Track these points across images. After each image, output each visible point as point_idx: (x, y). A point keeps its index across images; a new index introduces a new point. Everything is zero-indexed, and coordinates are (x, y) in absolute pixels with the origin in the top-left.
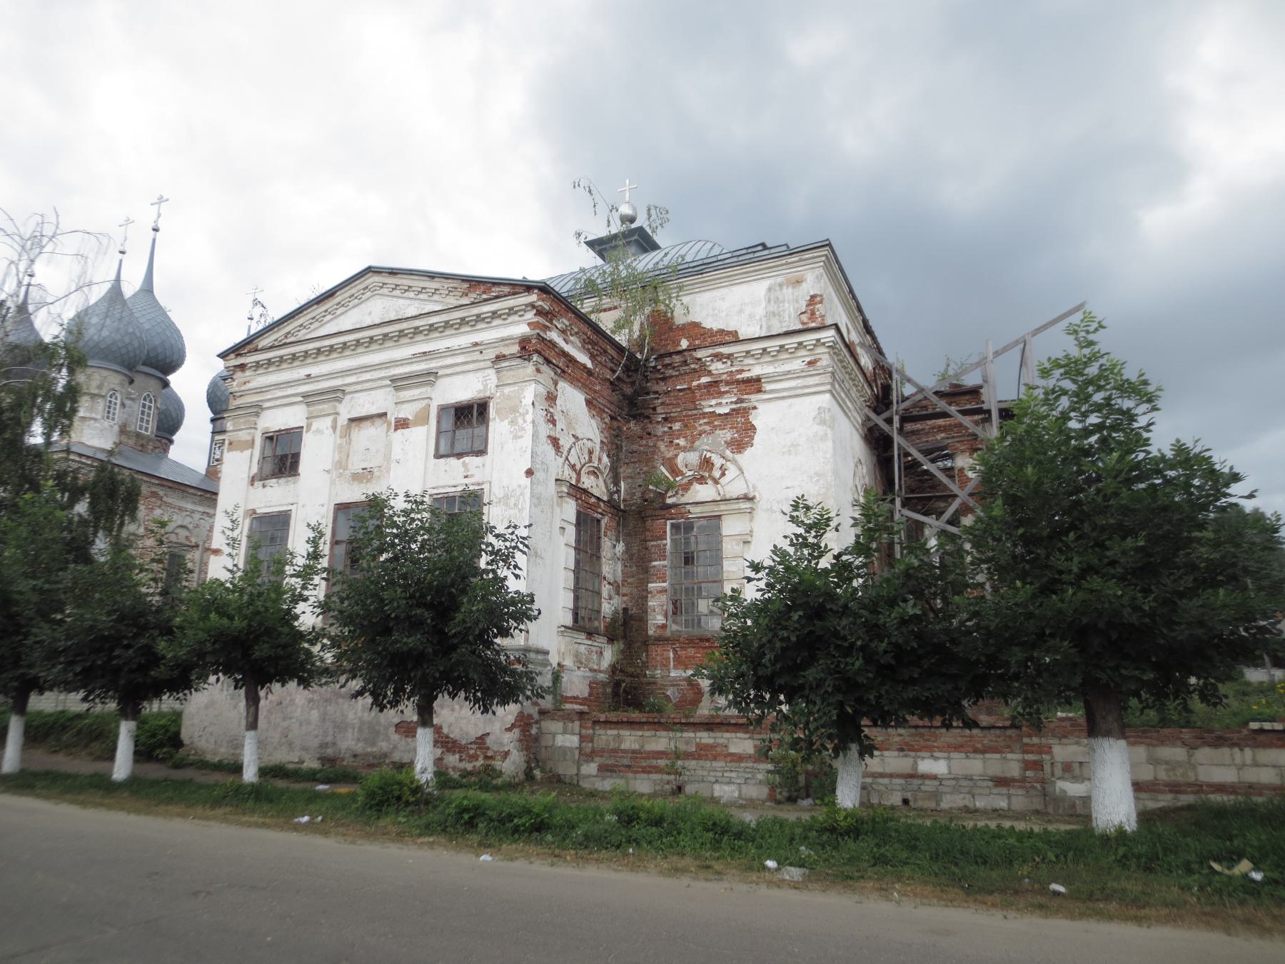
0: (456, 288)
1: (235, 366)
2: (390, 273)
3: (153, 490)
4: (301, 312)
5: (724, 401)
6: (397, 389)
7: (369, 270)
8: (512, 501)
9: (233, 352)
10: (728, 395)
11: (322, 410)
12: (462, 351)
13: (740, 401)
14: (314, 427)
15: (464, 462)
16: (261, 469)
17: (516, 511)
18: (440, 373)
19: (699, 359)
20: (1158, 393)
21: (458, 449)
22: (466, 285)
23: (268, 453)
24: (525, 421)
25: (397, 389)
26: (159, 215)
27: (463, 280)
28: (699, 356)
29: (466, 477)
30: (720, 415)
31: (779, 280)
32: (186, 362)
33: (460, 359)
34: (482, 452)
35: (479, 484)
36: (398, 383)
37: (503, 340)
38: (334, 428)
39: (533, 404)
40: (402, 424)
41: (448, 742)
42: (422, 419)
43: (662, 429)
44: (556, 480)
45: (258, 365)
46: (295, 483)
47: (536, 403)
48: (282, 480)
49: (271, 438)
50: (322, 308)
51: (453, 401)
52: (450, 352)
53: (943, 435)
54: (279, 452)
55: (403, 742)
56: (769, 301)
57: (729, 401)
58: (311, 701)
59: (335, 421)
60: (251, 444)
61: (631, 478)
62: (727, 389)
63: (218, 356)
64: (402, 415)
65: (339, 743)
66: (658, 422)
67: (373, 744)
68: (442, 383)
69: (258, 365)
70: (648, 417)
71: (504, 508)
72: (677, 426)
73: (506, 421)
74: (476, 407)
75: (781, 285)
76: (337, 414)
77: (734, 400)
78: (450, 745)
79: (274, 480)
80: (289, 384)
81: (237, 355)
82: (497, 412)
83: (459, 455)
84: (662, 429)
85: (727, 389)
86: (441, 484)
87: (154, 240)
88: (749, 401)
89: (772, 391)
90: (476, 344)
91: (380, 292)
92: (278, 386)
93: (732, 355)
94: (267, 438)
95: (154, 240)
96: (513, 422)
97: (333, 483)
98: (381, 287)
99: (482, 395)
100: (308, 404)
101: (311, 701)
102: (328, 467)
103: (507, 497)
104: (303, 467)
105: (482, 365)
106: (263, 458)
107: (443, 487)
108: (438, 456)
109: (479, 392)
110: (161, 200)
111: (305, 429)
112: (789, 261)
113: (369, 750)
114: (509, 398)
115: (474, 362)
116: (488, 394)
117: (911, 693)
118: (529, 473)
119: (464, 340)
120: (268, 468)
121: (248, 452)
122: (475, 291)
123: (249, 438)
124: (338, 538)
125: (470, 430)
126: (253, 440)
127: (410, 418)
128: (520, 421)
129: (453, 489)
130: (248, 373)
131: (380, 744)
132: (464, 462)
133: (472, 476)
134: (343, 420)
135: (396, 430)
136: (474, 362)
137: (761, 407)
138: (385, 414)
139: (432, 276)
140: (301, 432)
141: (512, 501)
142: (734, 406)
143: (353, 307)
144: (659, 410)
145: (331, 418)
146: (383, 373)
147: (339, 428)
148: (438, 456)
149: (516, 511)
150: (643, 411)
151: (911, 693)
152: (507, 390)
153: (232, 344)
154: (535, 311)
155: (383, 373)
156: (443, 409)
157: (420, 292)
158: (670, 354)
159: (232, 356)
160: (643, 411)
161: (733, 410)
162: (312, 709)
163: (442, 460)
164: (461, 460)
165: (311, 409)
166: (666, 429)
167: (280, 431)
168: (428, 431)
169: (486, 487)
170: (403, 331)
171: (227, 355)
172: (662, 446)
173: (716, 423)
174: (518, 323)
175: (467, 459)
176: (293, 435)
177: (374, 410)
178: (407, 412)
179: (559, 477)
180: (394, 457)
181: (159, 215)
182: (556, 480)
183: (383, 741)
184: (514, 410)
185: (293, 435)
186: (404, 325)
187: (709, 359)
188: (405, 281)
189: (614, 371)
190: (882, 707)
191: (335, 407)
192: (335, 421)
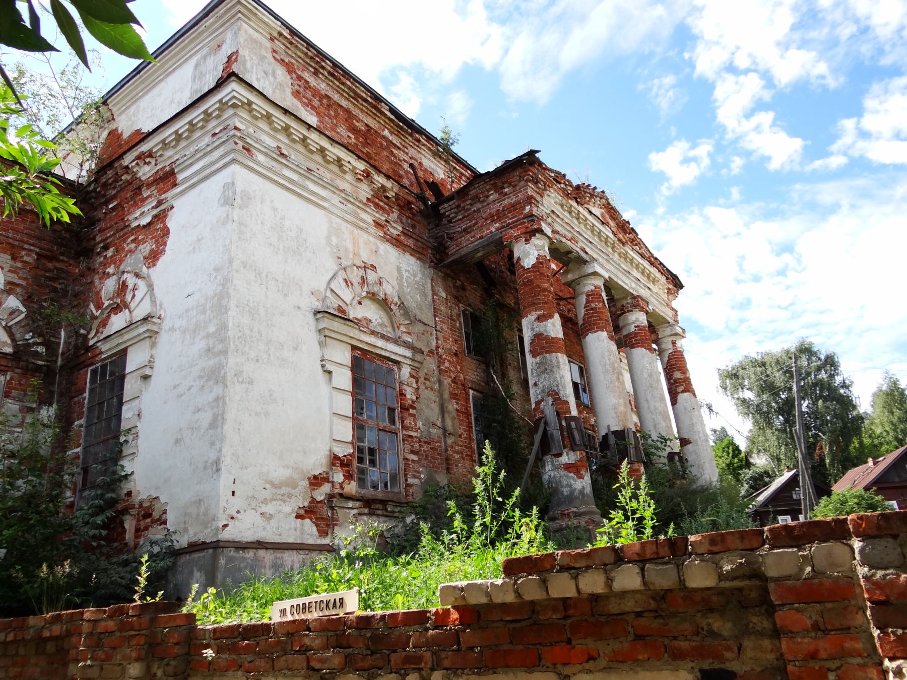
5: (146, 209)
7: (676, 311)
10: (150, 200)
13: (160, 203)
19: (127, 167)
20: (458, 137)
30: (144, 227)
31: (205, 51)
53: (497, 225)
56: (195, 78)
57: (150, 207)
60: (367, 607)
62: (149, 193)
75: (205, 57)
77: (154, 204)
85: (149, 193)
88: (167, 200)
89: (186, 180)
93: (150, 151)
112: (207, 24)
117: (516, 388)
137: (176, 203)
142: (155, 212)
151: (516, 388)
161: (155, 217)
173: (140, 238)
187: (134, 164)
190: (837, 402)
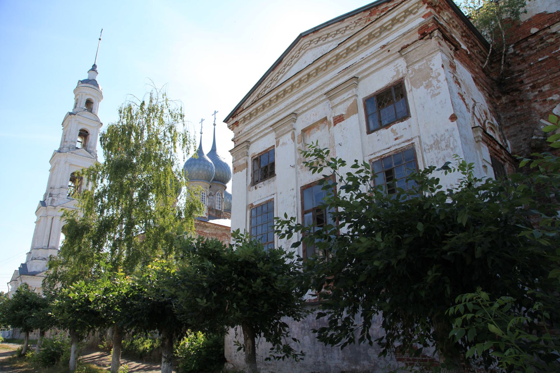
0: (360, 19)
1: (233, 124)
2: (314, 32)
3: (224, 232)
4: (264, 79)
6: (330, 99)
7: (302, 36)
8: (443, 144)
9: (231, 117)
11: (285, 130)
12: (374, 55)
14: (281, 143)
15: (392, 130)
16: (253, 179)
17: (449, 150)
18: (360, 77)
21: (385, 122)
22: (368, 13)
23: (256, 168)
24: (439, 81)
25: (330, 99)
26: (215, 119)
27: (365, 11)
28: (554, 31)
29: (396, 139)
32: (227, 163)
33: (375, 61)
34: (406, 115)
35: (409, 140)
36: (330, 95)
37: (404, 34)
38: (293, 138)
39: (443, 66)
40: (339, 119)
41: (426, 361)
42: (353, 110)
43: (533, 94)
44: (472, 128)
45: (245, 119)
46: (274, 181)
47: (445, 66)
48: (266, 182)
49: (256, 159)
50: (277, 70)
51: (374, 91)
52: (365, 60)
54: (262, 166)
55: (382, 361)
58: (303, 329)
59: (293, 134)
61: (515, 135)
63: (224, 121)
64: (338, 114)
65: (328, 362)
66: (528, 91)
67: (357, 362)
68: (361, 85)
69: (245, 119)
70: (517, 90)
71: (436, 151)
72: (546, 88)
73: (422, 87)
74: (393, 88)
76: (294, 129)
78: (428, 363)
79: (262, 183)
80: (262, 123)
81: (233, 118)
82: (413, 84)
83: (387, 126)
84: (533, 94)
86: (379, 149)
87: (214, 129)
90: (384, 46)
91: (310, 47)
92: (257, 126)
94: (254, 159)
95: (214, 129)
96: (427, 87)
97: (297, 173)
98: (310, 44)
99: (396, 79)
100: (274, 130)
101: (303, 329)
102: (293, 163)
103: (437, 143)
104: (278, 169)
105: (391, 58)
106: (254, 172)
107: (379, 152)
108: (369, 132)
109: (393, 78)
110: (215, 112)
111: (275, 146)
113: (354, 368)
114: (420, 70)
115: (384, 59)
116: (401, 76)
118: (453, 118)
119: (375, 47)
120: (258, 176)
121: (245, 171)
122: (375, 14)
123: (244, 162)
124: (306, 209)
125: (391, 107)
126: (247, 163)
127: (344, 113)
128: (434, 82)
129: (388, 151)
130: (241, 126)
131: (362, 362)
132: (392, 130)
133: (402, 136)
134: (298, 132)
135: (335, 125)
136: (384, 59)
138: (326, 118)
139: (341, 19)
140: (274, 150)
141: (443, 144)
143: (295, 63)
144: (526, 81)
145: (290, 133)
146: (319, 94)
147: (296, 138)
148: (369, 132)
149: (449, 150)
150: (512, 86)
152: (416, 66)
153: (230, 112)
154: (426, 5)
155: (319, 94)
156: (367, 101)
157: (336, 34)
158: (526, 39)
159: (231, 119)
160: (512, 86)
162: (305, 335)
163: (374, 134)
164: (390, 128)
165: (278, 132)
166: (537, 93)
167: (261, 153)
168: (359, 117)
169: (416, 141)
170: (328, 61)
171: (229, 119)
172: (537, 106)
174: (414, 19)
175: (394, 126)
176: (270, 153)
177: (318, 118)
178: (341, 110)
179: (473, 126)
180: (336, 143)
181: (215, 119)
182: (472, 128)
183: (364, 360)
184: (427, 77)
185: (270, 153)
186: (329, 57)
188: (323, 32)
189: (483, 63)
191: (292, 125)
192: (293, 134)
